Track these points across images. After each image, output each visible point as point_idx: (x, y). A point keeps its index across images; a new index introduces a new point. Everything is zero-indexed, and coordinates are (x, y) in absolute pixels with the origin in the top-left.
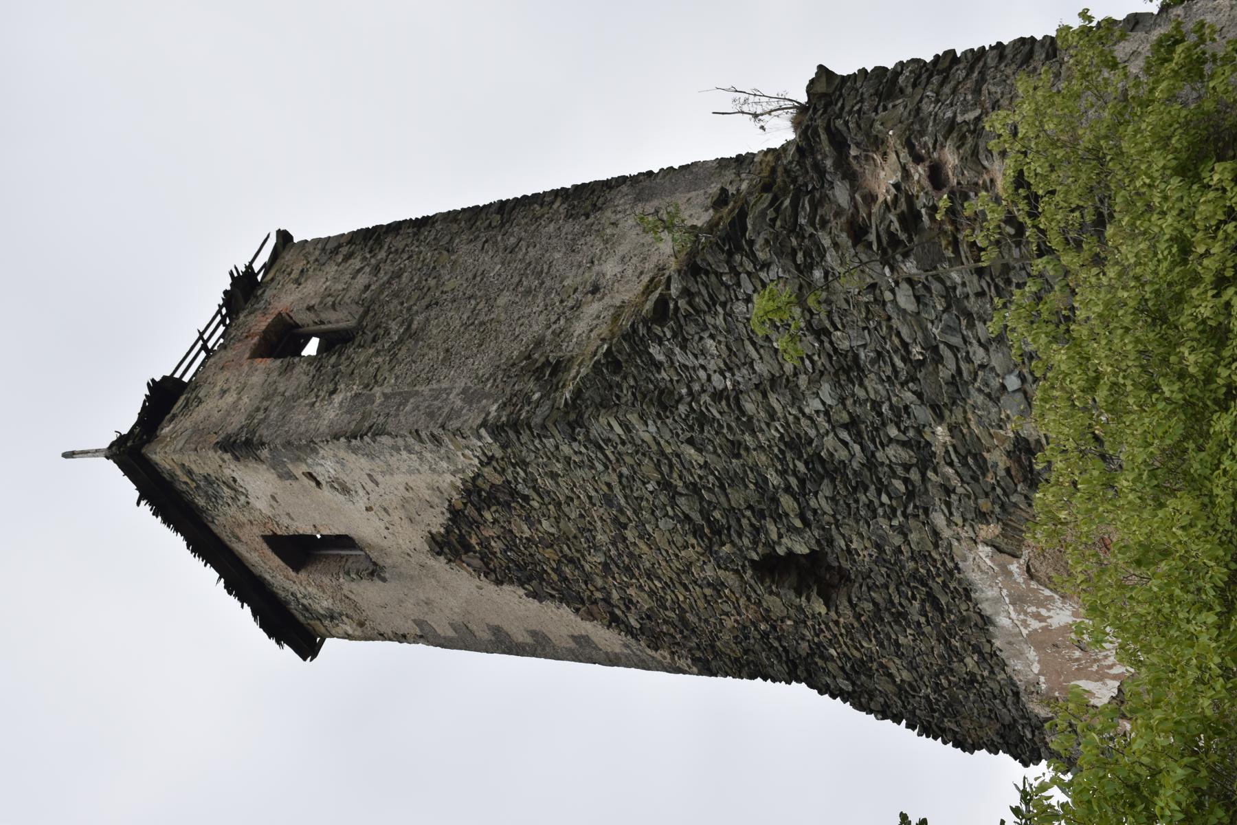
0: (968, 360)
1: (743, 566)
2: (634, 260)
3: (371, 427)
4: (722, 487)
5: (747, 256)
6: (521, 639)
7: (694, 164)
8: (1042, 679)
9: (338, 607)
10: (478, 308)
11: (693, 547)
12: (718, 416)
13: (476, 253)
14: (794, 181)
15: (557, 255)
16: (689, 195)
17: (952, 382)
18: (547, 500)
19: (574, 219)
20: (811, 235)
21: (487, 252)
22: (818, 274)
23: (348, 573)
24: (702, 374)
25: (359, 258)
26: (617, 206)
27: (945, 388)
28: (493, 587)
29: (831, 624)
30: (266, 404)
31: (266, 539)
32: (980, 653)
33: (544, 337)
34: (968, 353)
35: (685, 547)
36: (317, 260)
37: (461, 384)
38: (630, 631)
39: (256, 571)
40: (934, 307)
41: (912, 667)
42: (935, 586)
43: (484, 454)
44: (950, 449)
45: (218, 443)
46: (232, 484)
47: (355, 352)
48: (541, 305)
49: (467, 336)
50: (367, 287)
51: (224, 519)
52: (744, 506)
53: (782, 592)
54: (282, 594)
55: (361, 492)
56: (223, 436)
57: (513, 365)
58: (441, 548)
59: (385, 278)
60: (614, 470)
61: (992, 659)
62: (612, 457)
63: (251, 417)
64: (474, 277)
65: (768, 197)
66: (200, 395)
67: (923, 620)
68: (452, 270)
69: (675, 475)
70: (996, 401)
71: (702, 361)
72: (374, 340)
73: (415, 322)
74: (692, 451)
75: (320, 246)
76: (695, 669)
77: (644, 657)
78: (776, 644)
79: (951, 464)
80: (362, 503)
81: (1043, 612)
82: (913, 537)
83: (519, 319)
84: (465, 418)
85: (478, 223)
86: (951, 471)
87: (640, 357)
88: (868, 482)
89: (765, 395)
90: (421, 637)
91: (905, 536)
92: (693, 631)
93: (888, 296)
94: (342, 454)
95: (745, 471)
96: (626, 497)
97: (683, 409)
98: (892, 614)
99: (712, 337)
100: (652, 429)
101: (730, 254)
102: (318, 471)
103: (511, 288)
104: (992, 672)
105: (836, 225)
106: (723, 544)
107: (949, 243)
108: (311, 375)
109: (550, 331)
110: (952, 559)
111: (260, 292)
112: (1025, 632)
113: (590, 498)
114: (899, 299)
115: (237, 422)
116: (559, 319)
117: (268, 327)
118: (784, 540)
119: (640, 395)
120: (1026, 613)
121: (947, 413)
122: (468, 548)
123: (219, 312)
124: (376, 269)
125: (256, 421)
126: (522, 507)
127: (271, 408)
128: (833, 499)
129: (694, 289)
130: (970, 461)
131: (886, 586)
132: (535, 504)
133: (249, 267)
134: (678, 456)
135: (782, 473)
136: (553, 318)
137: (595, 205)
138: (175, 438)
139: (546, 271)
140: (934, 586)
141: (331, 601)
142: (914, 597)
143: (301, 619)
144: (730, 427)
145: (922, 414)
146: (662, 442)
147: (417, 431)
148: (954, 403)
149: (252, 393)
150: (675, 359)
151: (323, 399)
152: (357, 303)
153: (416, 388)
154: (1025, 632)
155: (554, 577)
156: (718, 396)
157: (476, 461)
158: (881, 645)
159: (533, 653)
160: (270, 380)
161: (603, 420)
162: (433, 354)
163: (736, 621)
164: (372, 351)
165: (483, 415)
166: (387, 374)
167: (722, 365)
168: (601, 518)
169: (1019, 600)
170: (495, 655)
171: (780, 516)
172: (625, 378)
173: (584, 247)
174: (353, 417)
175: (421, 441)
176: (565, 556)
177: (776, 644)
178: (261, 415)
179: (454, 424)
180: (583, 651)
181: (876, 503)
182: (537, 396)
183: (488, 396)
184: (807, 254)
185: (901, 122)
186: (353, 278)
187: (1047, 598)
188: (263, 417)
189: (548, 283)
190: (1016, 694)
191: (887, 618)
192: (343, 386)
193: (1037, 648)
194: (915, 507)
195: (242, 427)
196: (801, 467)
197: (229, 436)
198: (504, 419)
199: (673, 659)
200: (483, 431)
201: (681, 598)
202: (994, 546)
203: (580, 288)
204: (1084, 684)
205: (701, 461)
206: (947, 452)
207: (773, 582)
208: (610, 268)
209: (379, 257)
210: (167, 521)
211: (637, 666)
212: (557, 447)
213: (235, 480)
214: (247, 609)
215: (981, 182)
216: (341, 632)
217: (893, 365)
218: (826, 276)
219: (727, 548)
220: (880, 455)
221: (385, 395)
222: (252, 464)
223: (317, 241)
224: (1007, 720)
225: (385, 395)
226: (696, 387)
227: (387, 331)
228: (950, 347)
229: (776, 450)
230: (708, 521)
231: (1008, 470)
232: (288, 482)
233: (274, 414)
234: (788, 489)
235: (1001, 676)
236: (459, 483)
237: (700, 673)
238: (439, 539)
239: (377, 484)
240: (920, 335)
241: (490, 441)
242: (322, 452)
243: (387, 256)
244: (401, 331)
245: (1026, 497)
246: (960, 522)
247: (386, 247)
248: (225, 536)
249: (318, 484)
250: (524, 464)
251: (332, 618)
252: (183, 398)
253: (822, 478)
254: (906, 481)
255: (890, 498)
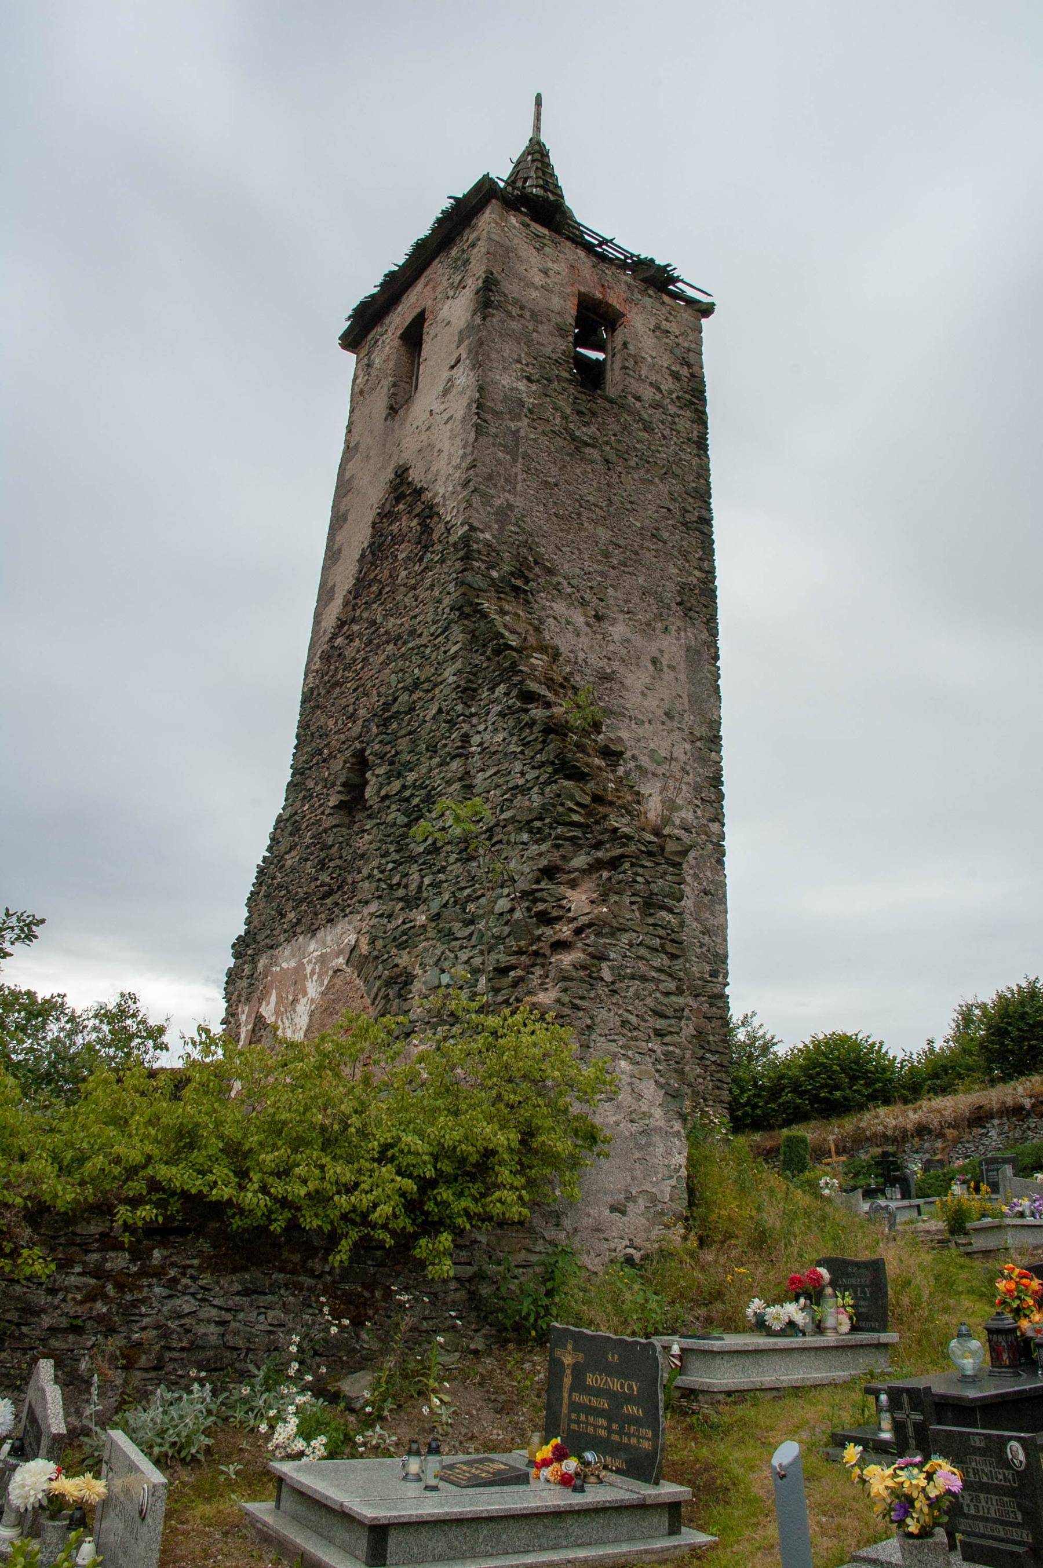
0: (461, 948)
1: (362, 742)
2: (624, 651)
3: (485, 421)
4: (411, 733)
5: (549, 778)
6: (338, 539)
7: (719, 698)
8: (278, 969)
9: (374, 372)
10: (597, 509)
11: (378, 701)
12: (452, 737)
13: (658, 502)
14: (597, 823)
15: (641, 580)
16: (685, 696)
17: (450, 933)
18: (419, 577)
19: (679, 591)
20: (550, 834)
21: (657, 512)
22: (525, 837)
23: (394, 385)
24: (481, 728)
25: (673, 387)
26: (685, 631)
27: (447, 925)
28: (371, 519)
29: (322, 809)
30: (527, 315)
31: (423, 312)
32: (296, 924)
33: (555, 575)
34: (466, 948)
35: (379, 695)
36: (678, 345)
37: (518, 502)
38: (334, 636)
39: (404, 299)
40: (495, 926)
41: (293, 869)
42: (336, 897)
43: (453, 526)
44: (412, 924)
45: (492, 274)
46: (461, 285)
47: (569, 397)
48: (591, 569)
49: (569, 502)
50: (638, 399)
51: (439, 271)
52: (399, 749)
53: (344, 771)
54: (387, 321)
55: (442, 407)
56: (499, 277)
57: (531, 549)
58: (399, 476)
59: (645, 416)
60: (430, 641)
61: (292, 933)
62: (436, 642)
63: (516, 302)
64: (631, 503)
65: (587, 800)
66: (546, 249)
67: (318, 883)
68: (643, 481)
69: (421, 694)
70: (436, 964)
71: (490, 728)
72: (579, 413)
73: (592, 451)
74: (434, 712)
75: (693, 346)
76: (306, 690)
77: (317, 647)
78: (314, 761)
79: (404, 923)
80: (437, 407)
81: (315, 977)
82: (366, 884)
83: (579, 549)
84: (481, 511)
85: (691, 500)
86: (400, 921)
87: (499, 675)
88: (401, 854)
89: (460, 779)
90: (348, 447)
91: (367, 878)
92: (329, 692)
93: (506, 891)
94: (468, 393)
95: (417, 754)
96: (413, 648)
97: (460, 708)
98: (324, 859)
99: (504, 740)
100: (451, 679)
101: (553, 763)
102: (460, 368)
103: (613, 539)
104: (285, 931)
105: (555, 857)
106: (378, 727)
107: (520, 948)
108: (552, 355)
109: (561, 580)
110: (351, 913)
111: (651, 292)
112: (305, 961)
113: (415, 617)
114: (503, 899)
115: (511, 289)
116: (573, 587)
117: (611, 305)
118: (374, 779)
119: (475, 671)
120: (315, 964)
121: (433, 925)
122: (398, 499)
123: (632, 255)
124: (656, 405)
125: (510, 308)
126: (417, 555)
127: (523, 321)
128: (395, 824)
129: (535, 729)
130: (405, 938)
131: (341, 858)
132: (416, 568)
133: (677, 280)
134: (433, 698)
135: (414, 786)
136: (574, 582)
137: (690, 610)
138: (503, 230)
139: (626, 569)
140: (337, 896)
141: (378, 366)
142: (332, 878)
143: (370, 337)
144: (445, 746)
145: (435, 906)
146: (442, 687)
147: (475, 466)
148: (439, 932)
149: (542, 301)
150: (494, 705)
151: (522, 370)
152: (623, 391)
153: (520, 460)
154: (305, 961)
155: (372, 576)
156: (466, 739)
157: (448, 519)
158: (307, 847)
159: (329, 549)
160: (552, 315)
161: (460, 637)
162: (555, 470)
163: (331, 730)
164: (568, 411)
165: (481, 527)
166: (540, 430)
167: (485, 745)
168: (402, 624)
169: (323, 959)
170: (330, 514)
171: (389, 778)
172: (489, 659)
173: (645, 604)
174: (499, 404)
175: (468, 469)
176: (383, 588)
177: (314, 761)
178: (515, 311)
179: (476, 500)
180: (326, 593)
181: (389, 859)
182: (495, 574)
183: (501, 530)
184: (540, 830)
185: (615, 917)
186: (651, 384)
187: (323, 981)
188: (514, 314)
189: (613, 573)
190: (271, 947)
191: (323, 855)
192: (534, 388)
193: (295, 968)
194: (384, 889)
195: (506, 296)
196: (415, 801)
197: (497, 283)
198: (475, 546)
199: (313, 671)
200: (466, 528)
201: (349, 685)
202: (355, 946)
203: (602, 604)
204: (273, 998)
205: (427, 719)
206: (411, 921)
207: (353, 764)
208: (619, 630)
209: (670, 407)
210: (439, 221)
211: (312, 639)
212: (449, 593)
213: (464, 288)
214: (375, 290)
215: (547, 981)
216: (359, 372)
217: (466, 888)
218: (523, 843)
219: (375, 730)
220: (415, 867)
221: (518, 430)
222: (472, 306)
223: (699, 343)
224: (259, 938)
225: (518, 430)
226: (475, 721)
227: (587, 424)
228: (471, 934)
229: (427, 782)
230: (391, 717)
231: (397, 966)
232: (456, 338)
233: (515, 325)
234: (404, 787)
235: (282, 938)
236: (437, 500)
237: (303, 693)
238: (405, 475)
239: (445, 423)
240: (480, 912)
241: (460, 533)
242: (472, 374)
243: (670, 415)
244: (585, 438)
245: (380, 977)
246: (371, 923)
247: (680, 412)
248: (429, 272)
249: (452, 367)
250: (442, 561)
251: (368, 366)
252: (546, 232)
253: (408, 816)
254: (399, 884)
255: (391, 870)
